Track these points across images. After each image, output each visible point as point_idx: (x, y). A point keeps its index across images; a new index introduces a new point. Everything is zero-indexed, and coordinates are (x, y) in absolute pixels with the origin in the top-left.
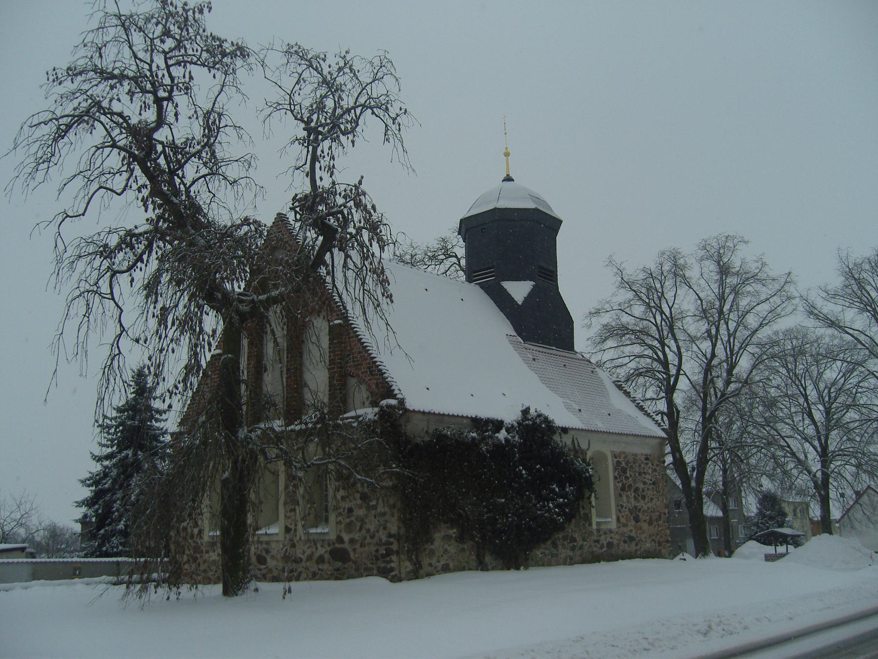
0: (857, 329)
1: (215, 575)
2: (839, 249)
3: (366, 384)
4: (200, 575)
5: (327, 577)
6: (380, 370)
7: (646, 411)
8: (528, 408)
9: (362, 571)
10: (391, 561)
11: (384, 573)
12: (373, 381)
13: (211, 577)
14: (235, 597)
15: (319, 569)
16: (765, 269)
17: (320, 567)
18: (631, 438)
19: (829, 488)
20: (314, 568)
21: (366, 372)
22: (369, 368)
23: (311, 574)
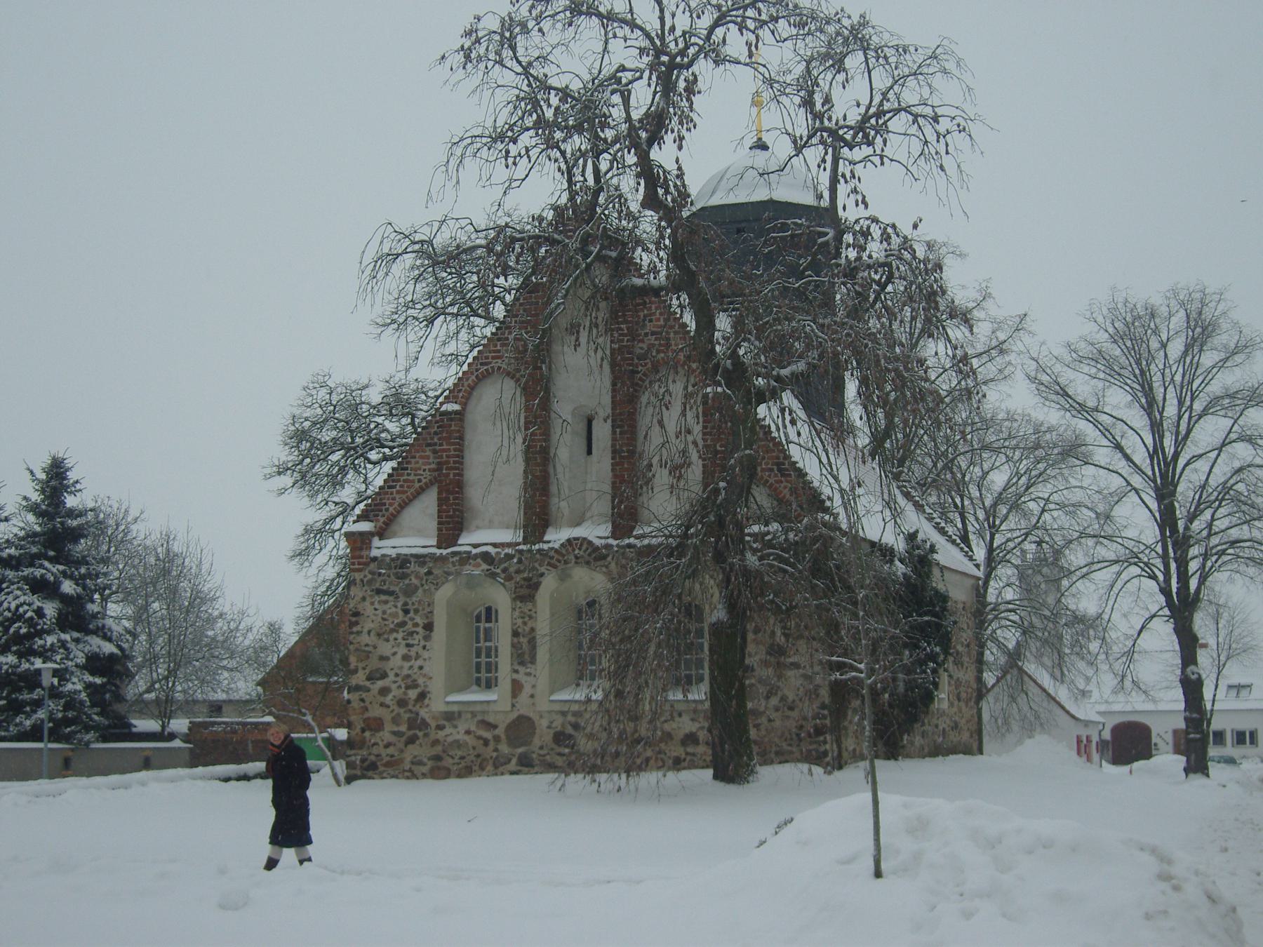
0: (1120, 417)
1: (458, 764)
2: (1114, 288)
3: (764, 485)
4: (425, 765)
5: (705, 764)
6: (800, 470)
7: (950, 537)
8: (917, 531)
9: (773, 755)
10: (825, 742)
11: (816, 758)
12: (785, 484)
13: (451, 767)
14: (746, 785)
15: (687, 754)
16: (988, 304)
17: (690, 750)
18: (958, 577)
19: (280, 660)
20: (679, 751)
21: (771, 470)
22: (778, 464)
23: (671, 761)
